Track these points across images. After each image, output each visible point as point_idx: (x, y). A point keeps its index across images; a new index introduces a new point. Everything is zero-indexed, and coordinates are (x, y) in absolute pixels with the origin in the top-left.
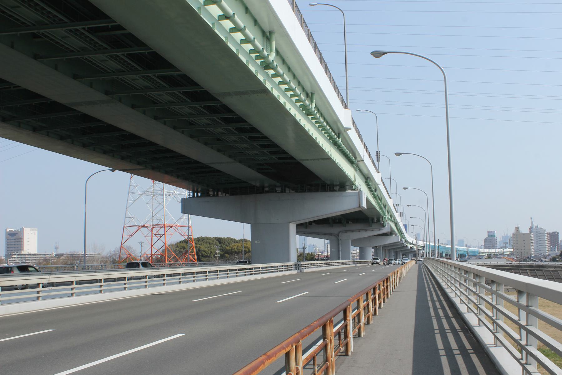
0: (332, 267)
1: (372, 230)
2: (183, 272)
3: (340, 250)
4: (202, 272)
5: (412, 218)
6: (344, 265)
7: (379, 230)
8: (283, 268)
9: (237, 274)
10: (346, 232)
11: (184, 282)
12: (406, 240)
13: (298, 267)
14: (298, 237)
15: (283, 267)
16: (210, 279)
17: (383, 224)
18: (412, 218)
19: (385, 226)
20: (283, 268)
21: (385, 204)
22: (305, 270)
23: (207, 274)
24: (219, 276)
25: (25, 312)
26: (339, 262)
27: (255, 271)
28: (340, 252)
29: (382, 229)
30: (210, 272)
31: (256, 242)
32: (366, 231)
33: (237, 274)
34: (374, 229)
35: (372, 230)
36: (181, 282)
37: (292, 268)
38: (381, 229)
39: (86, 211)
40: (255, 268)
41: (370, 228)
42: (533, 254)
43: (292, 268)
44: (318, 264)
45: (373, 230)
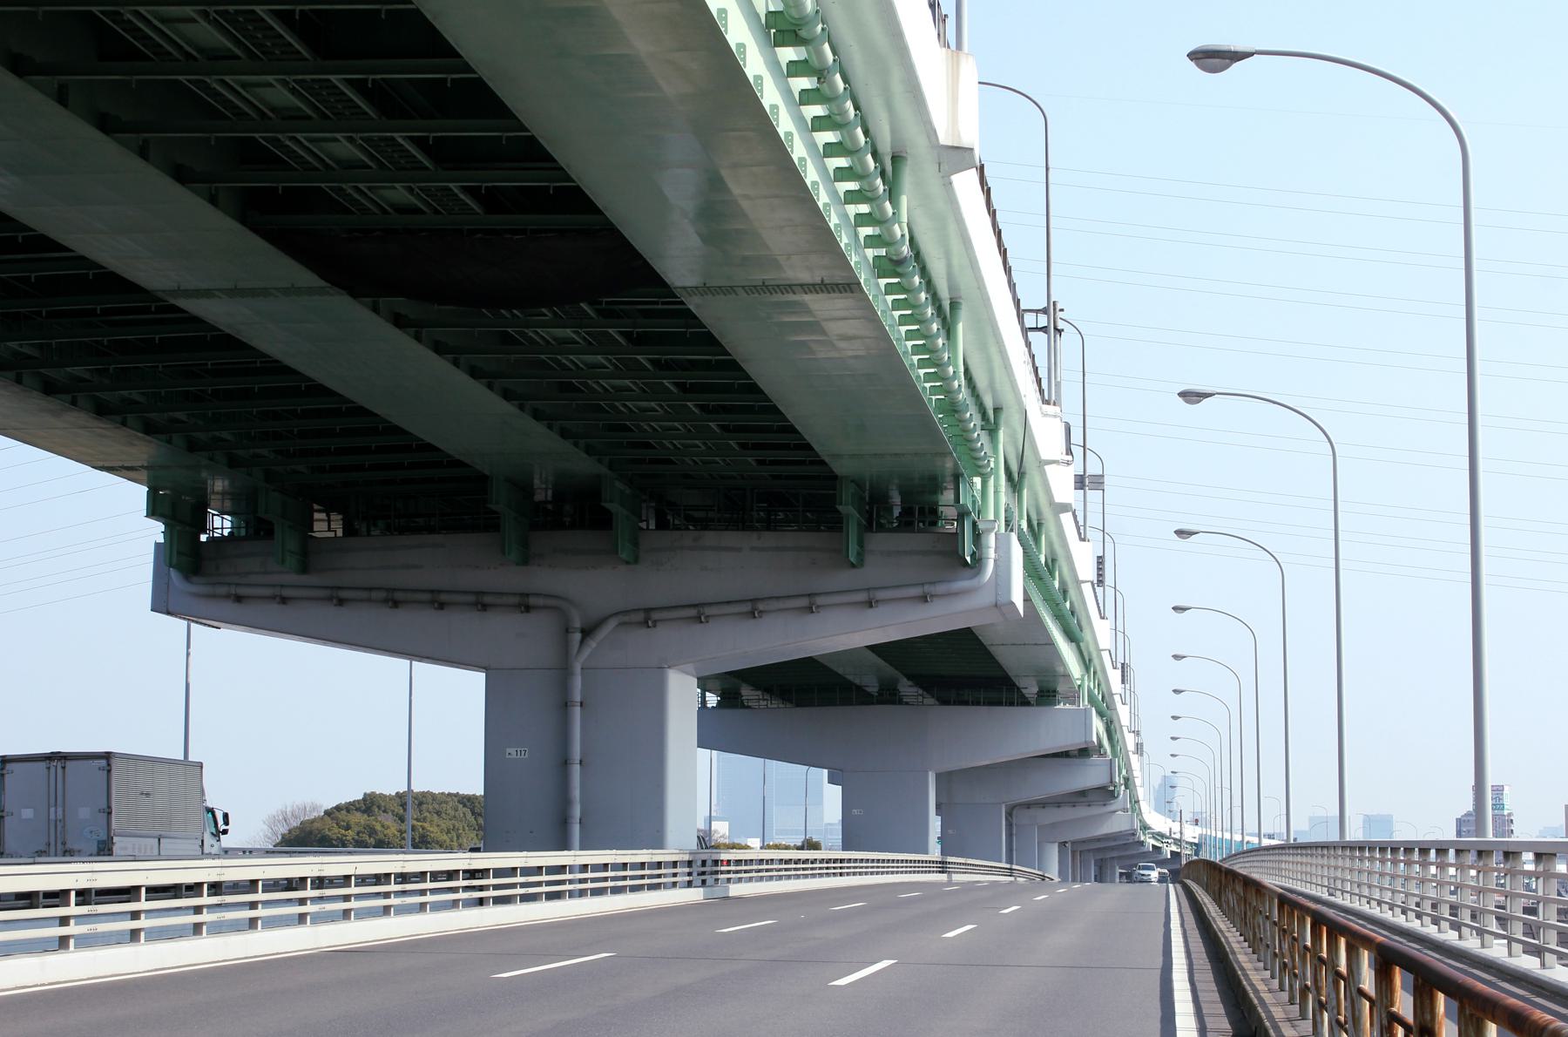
0: (792, 881)
1: (862, 597)
2: (83, 882)
3: (576, 751)
4: (37, 893)
5: (1192, 533)
6: (872, 873)
7: (1105, 805)
8: (675, 871)
9: (64, 931)
10: (647, 617)
11: (86, 942)
12: (1145, 827)
13: (703, 873)
14: (704, 754)
15: (660, 868)
16: (218, 929)
17: (956, 537)
18: (1192, 533)
19: (1119, 794)
20: (675, 871)
21: (952, 287)
22: (736, 890)
23: (73, 909)
24: (72, 929)
25: (148, 971)
26: (561, 869)
27: (496, 887)
28: (576, 770)
29: (1111, 804)
30: (84, 896)
31: (950, 832)
32: (1074, 806)
33: (64, 931)
34: (880, 595)
35: (862, 597)
36: (72, 942)
37: (675, 875)
38: (941, 588)
39: (191, 681)
40: (499, 873)
41: (845, 578)
42: (1091, 854)
43: (675, 875)
44: (584, 868)
45: (1089, 805)
